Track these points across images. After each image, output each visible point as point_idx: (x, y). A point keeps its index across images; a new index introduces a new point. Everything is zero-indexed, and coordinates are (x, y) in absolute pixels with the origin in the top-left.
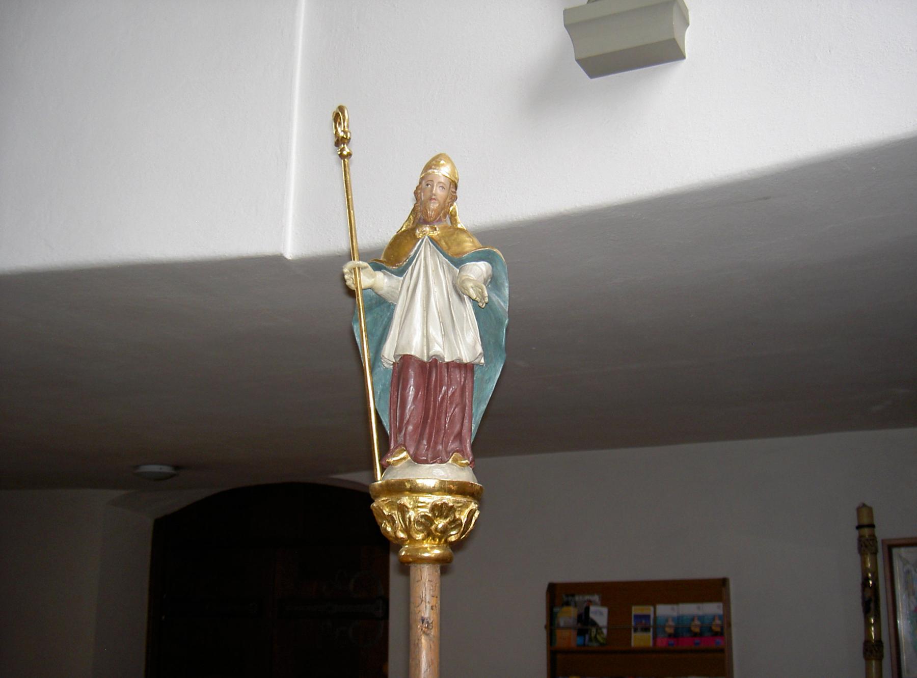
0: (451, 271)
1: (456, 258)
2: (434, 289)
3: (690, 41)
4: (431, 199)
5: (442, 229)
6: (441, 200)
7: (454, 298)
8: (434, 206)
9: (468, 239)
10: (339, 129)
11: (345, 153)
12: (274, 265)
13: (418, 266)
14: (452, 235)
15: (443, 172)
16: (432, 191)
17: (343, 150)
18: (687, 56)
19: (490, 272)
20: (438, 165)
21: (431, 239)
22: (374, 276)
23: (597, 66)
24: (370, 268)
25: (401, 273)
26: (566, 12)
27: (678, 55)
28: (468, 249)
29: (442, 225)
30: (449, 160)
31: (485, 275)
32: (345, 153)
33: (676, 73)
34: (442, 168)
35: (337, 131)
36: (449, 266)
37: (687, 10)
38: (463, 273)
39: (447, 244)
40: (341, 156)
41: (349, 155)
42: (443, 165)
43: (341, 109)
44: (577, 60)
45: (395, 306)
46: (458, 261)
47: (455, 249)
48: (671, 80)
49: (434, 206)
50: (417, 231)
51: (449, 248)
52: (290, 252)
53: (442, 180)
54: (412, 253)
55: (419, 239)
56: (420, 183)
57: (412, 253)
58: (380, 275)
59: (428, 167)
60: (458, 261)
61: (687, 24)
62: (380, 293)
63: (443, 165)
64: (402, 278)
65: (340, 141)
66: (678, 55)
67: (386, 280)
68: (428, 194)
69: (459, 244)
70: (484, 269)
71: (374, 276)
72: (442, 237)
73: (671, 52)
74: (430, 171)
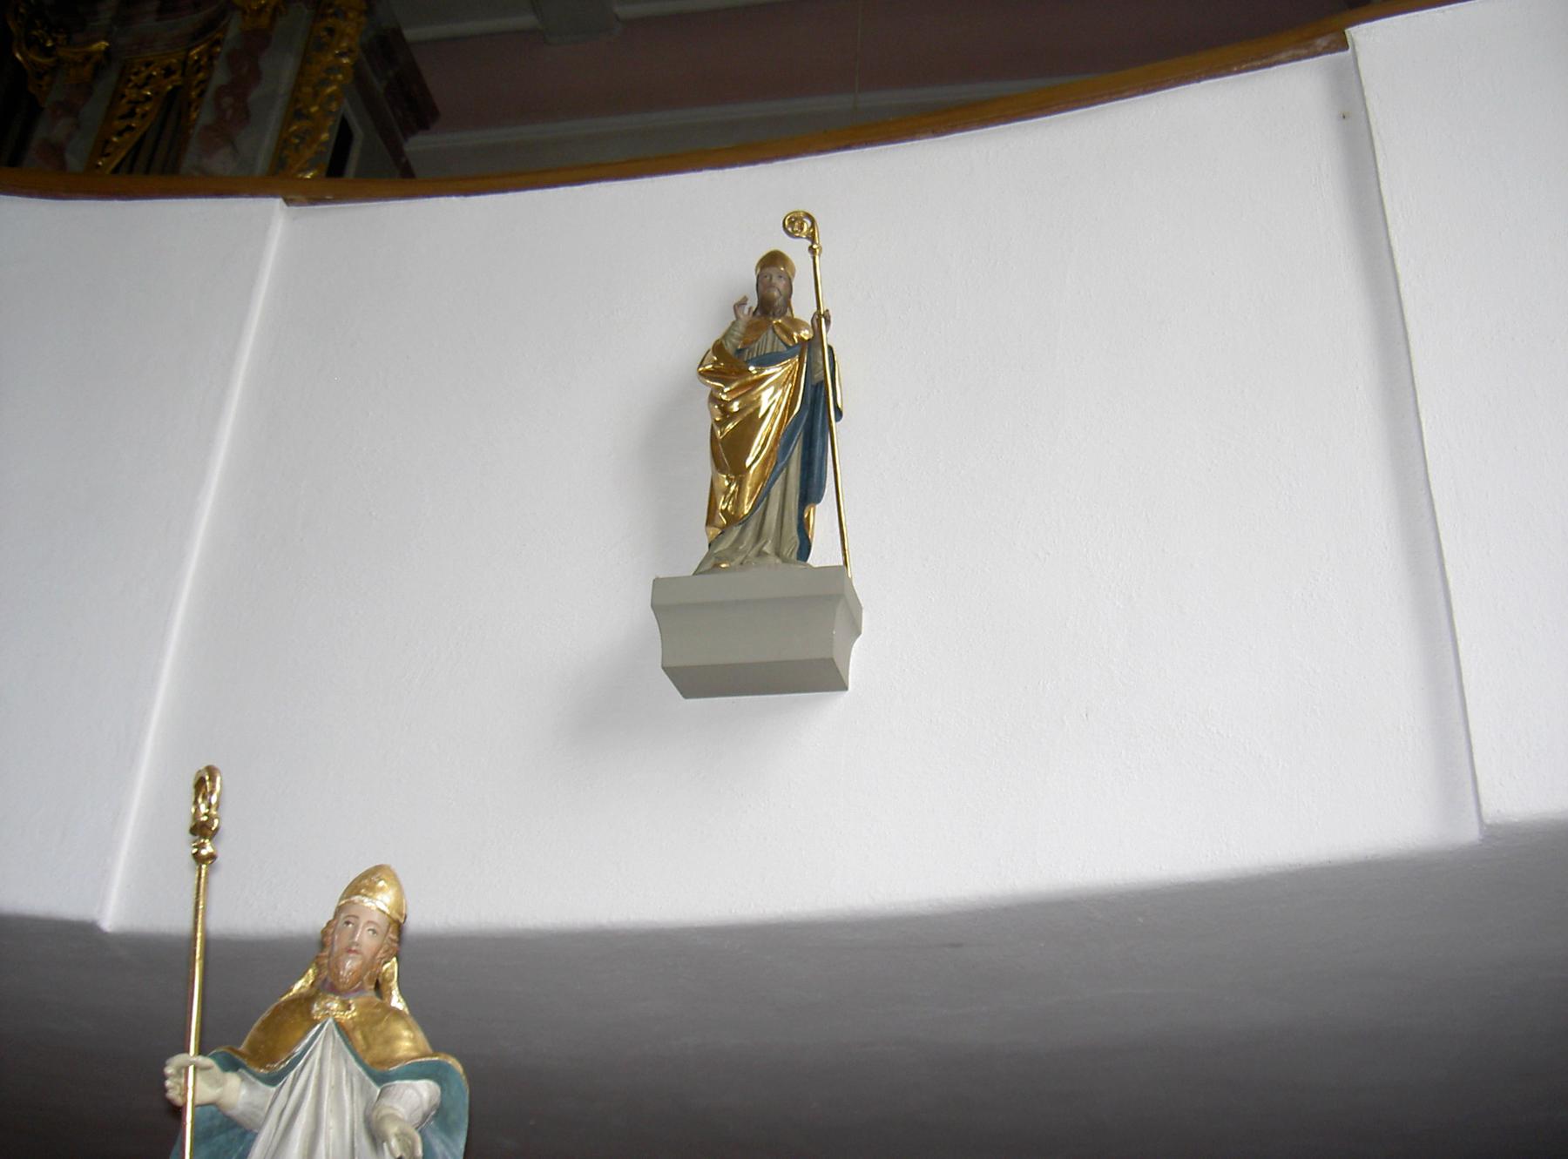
0: (364, 1090)
1: (378, 1070)
2: (329, 1123)
3: (860, 661)
4: (350, 951)
5: (360, 1007)
6: (368, 954)
7: (364, 1142)
8: (350, 964)
9: (406, 1033)
10: (203, 809)
11: (204, 852)
12: (83, 935)
13: (306, 1075)
14: (378, 1022)
15: (381, 902)
16: (353, 936)
17: (202, 846)
18: (852, 679)
19: (437, 1100)
20: (372, 889)
21: (340, 1026)
22: (220, 1083)
23: (695, 681)
24: (217, 1069)
25: (274, 1080)
26: (657, 583)
27: (836, 682)
28: (401, 1053)
29: (361, 1000)
30: (395, 880)
31: (426, 1107)
32: (204, 852)
33: (832, 706)
34: (379, 896)
35: (198, 809)
36: (362, 1081)
37: (860, 608)
38: (386, 1102)
39: (365, 1038)
40: (197, 858)
41: (212, 857)
42: (382, 889)
43: (211, 771)
44: (670, 671)
45: (256, 1135)
46: (381, 1073)
47: (378, 1051)
48: (816, 720)
49: (350, 964)
50: (316, 1007)
51: (369, 1047)
52: (112, 915)
53: (376, 918)
54: (298, 1050)
55: (316, 1022)
56: (336, 915)
57: (298, 1050)
58: (233, 1080)
59: (355, 888)
60: (381, 1073)
61: (859, 633)
62: (229, 1112)
63: (382, 889)
64: (274, 1089)
65: (201, 830)
66: (836, 682)
67: (244, 1092)
68: (345, 941)
69: (390, 1040)
70: (426, 1095)
71: (220, 1083)
72: (357, 1024)
73: (824, 676)
74: (356, 898)
